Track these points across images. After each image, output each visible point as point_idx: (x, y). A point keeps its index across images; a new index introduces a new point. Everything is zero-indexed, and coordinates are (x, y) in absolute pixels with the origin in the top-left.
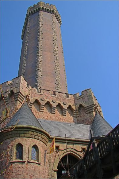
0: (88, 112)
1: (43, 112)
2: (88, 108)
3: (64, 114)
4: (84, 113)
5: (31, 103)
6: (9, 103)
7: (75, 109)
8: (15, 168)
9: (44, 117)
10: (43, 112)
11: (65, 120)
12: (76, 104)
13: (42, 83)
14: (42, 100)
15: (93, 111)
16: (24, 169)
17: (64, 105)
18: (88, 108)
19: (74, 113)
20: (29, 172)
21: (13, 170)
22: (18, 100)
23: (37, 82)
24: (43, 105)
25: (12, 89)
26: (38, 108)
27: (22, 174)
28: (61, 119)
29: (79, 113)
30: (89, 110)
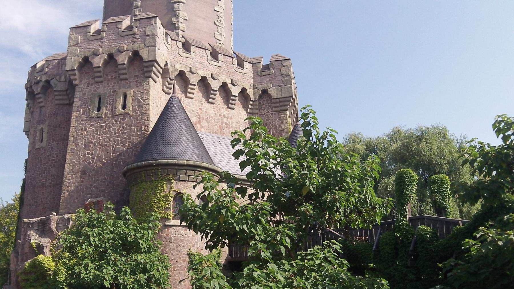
0: (278, 109)
1: (192, 98)
2: (280, 102)
3: (230, 105)
4: (268, 109)
5: (170, 79)
6: (130, 78)
7: (252, 97)
8: (175, 235)
9: (193, 111)
10: (192, 98)
11: (231, 118)
12: (255, 88)
13: (186, 20)
14: (193, 73)
15: (288, 110)
16: (188, 237)
17: (233, 86)
18: (280, 102)
19: (250, 106)
20: (196, 242)
21: (171, 238)
22: (150, 77)
23: (177, 16)
24: (195, 85)
25: (136, 46)
26: (183, 90)
27: (187, 246)
28: (224, 116)
29: (259, 106)
30: (280, 106)
